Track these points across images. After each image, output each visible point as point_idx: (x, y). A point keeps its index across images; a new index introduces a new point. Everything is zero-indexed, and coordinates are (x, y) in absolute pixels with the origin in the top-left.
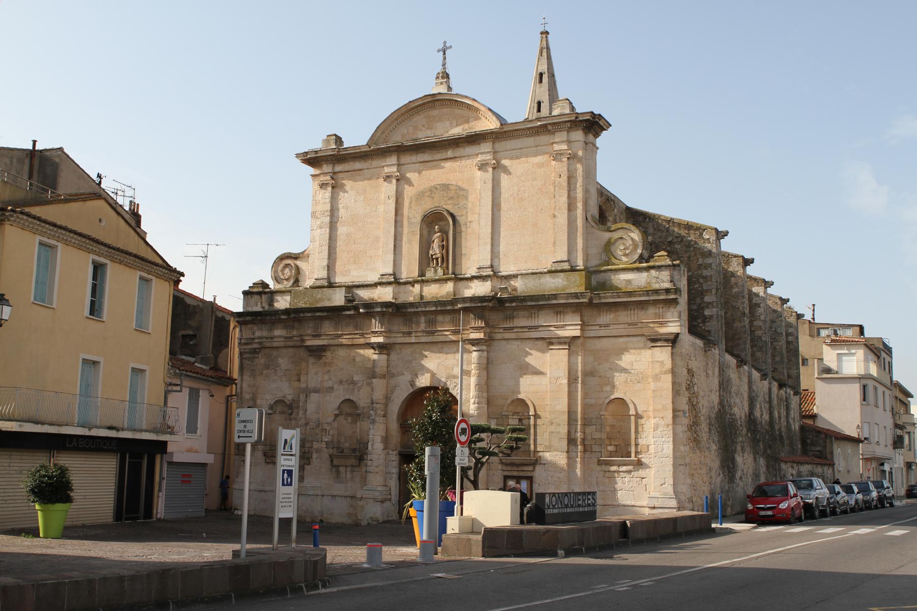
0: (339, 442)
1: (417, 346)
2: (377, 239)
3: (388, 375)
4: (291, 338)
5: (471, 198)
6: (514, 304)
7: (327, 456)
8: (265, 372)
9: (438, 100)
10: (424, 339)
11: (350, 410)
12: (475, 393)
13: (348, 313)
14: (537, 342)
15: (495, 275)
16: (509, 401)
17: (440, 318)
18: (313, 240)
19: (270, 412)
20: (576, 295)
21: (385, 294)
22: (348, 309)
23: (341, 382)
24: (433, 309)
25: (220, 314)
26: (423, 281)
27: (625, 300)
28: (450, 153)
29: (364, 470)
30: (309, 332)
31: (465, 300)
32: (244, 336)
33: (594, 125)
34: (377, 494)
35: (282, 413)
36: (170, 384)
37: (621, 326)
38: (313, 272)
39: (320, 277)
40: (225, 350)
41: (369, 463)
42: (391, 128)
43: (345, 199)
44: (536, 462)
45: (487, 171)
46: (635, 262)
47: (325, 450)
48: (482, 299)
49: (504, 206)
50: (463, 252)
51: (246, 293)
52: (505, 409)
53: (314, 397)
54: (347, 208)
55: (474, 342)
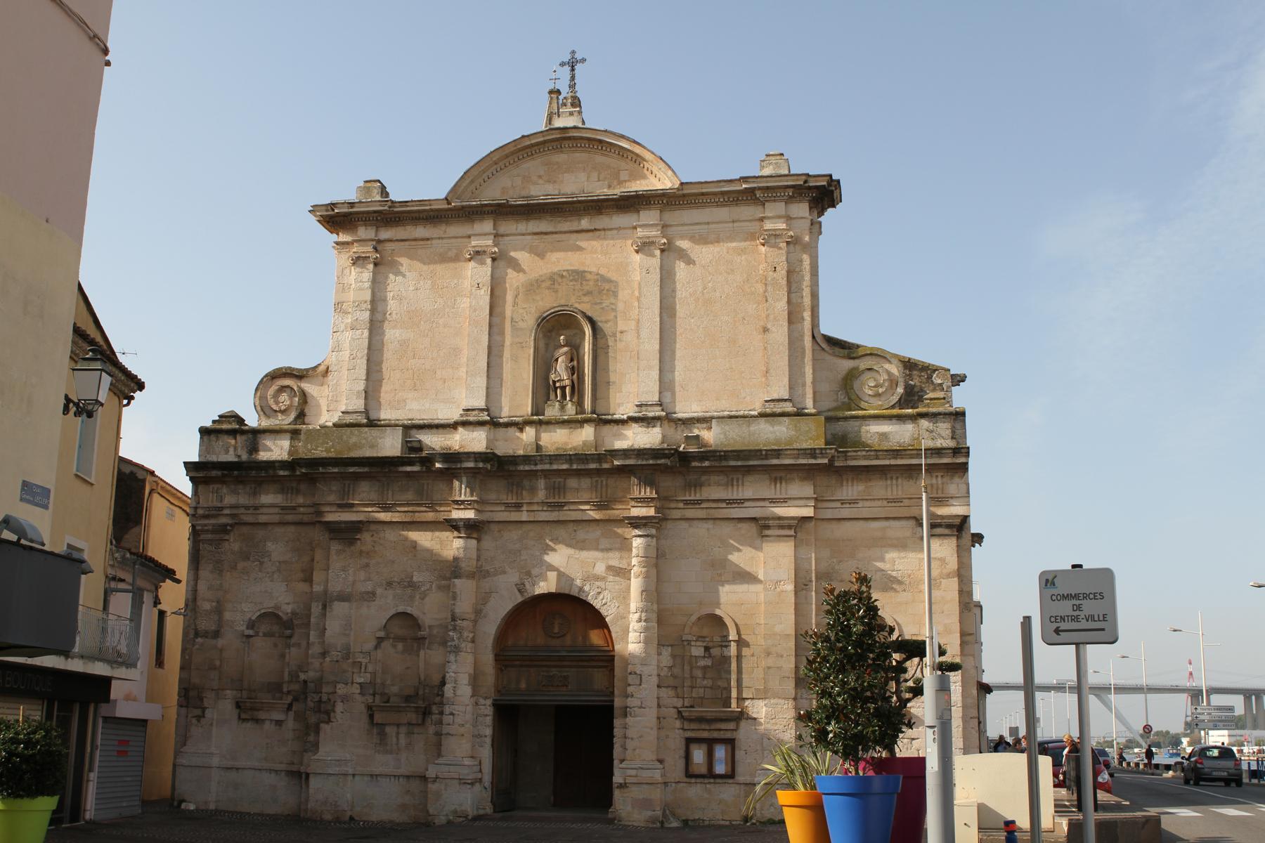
1: (529, 527)
2: (456, 351)
4: (294, 508)
5: (623, 294)
6: (707, 464)
7: (363, 708)
8: (241, 565)
9: (570, 138)
10: (543, 516)
11: (407, 630)
12: (640, 605)
13: (409, 469)
14: (740, 525)
15: (669, 419)
16: (694, 618)
17: (572, 482)
18: (337, 348)
19: (251, 632)
20: (812, 453)
21: (475, 441)
22: (410, 462)
24: (565, 467)
25: (127, 470)
26: (541, 423)
27: (887, 462)
28: (585, 223)
30: (332, 498)
31: (614, 453)
32: (203, 503)
35: (269, 635)
36: (114, 579)
37: (879, 503)
38: (333, 404)
39: (350, 408)
40: (135, 530)
43: (395, 285)
45: (654, 256)
46: (893, 407)
49: (681, 311)
51: (204, 432)
52: (687, 630)
53: (339, 608)
54: (400, 299)
55: (636, 523)
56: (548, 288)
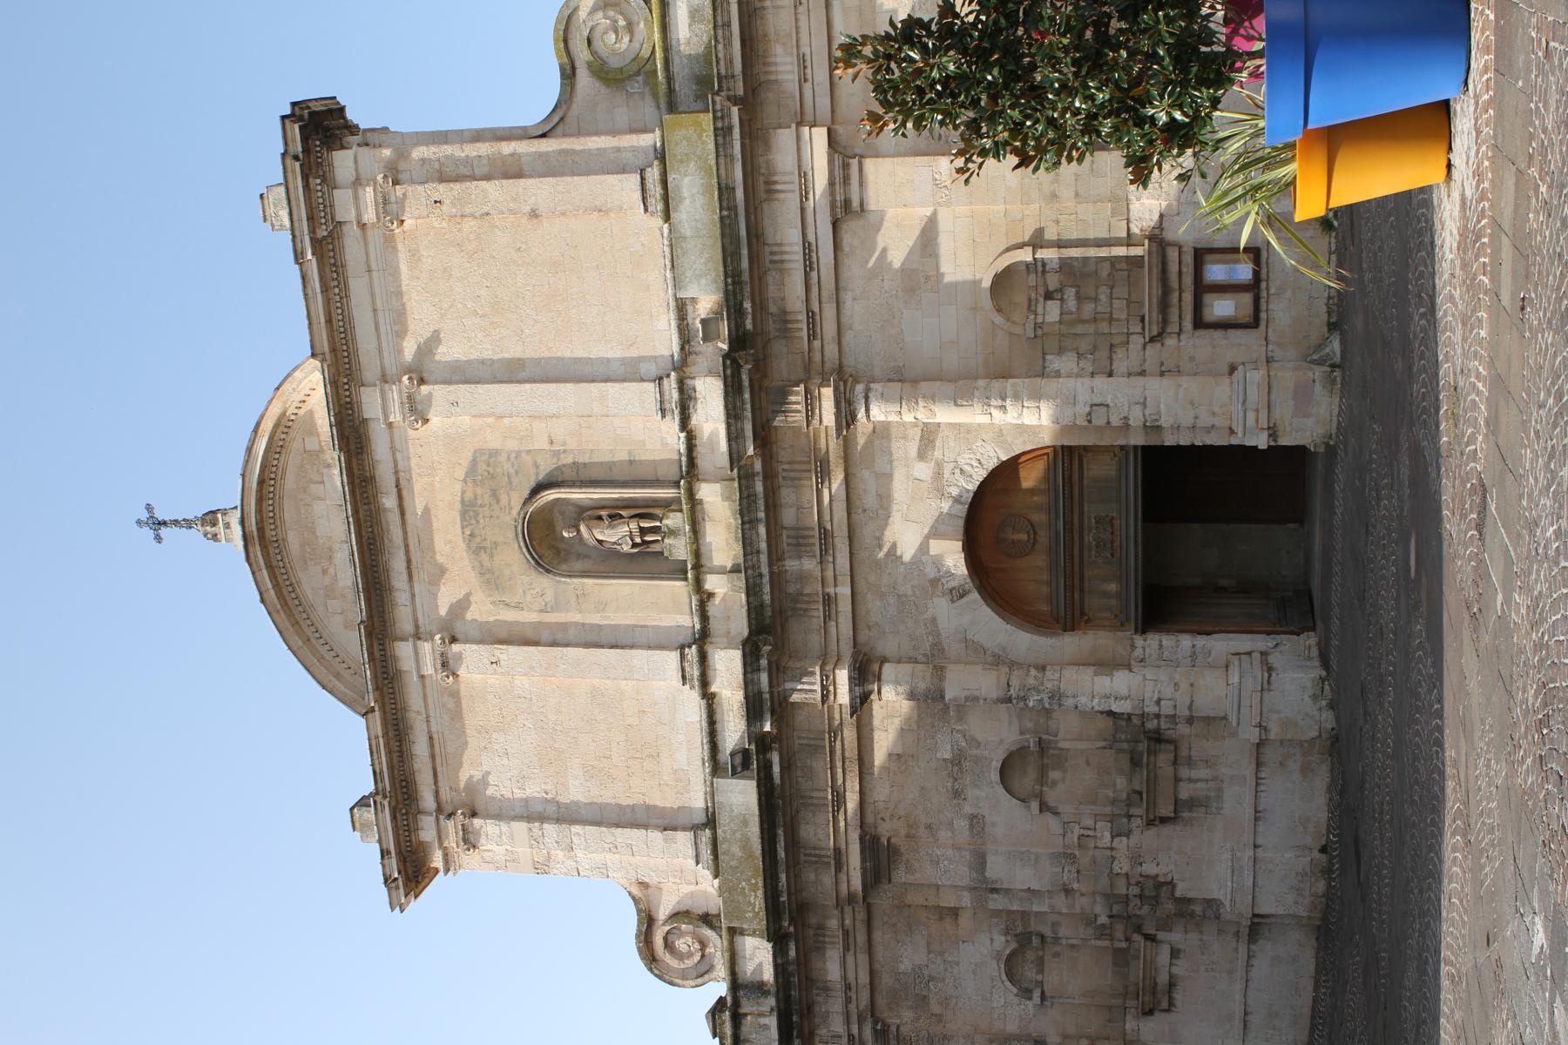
0: (1114, 802)
3: (935, 659)
4: (846, 933)
6: (747, 305)
9: (261, 530)
11: (1029, 768)
12: (978, 407)
13: (776, 769)
16: (998, 319)
17: (788, 517)
19: (1037, 994)
20: (722, 133)
21: (728, 665)
22: (766, 768)
23: (957, 794)
24: (762, 530)
26: (698, 566)
28: (389, 502)
29: (1184, 729)
30: (828, 880)
33: (319, 128)
34: (1249, 683)
35: (1040, 964)
37: (803, 19)
39: (691, 852)
41: (1166, 708)
42: (328, 656)
44: (1157, 239)
45: (430, 395)
47: (1134, 839)
48: (732, 390)
49: (513, 351)
50: (624, 456)
52: (1018, 330)
53: (997, 869)
55: (846, 418)
56: (492, 556)
